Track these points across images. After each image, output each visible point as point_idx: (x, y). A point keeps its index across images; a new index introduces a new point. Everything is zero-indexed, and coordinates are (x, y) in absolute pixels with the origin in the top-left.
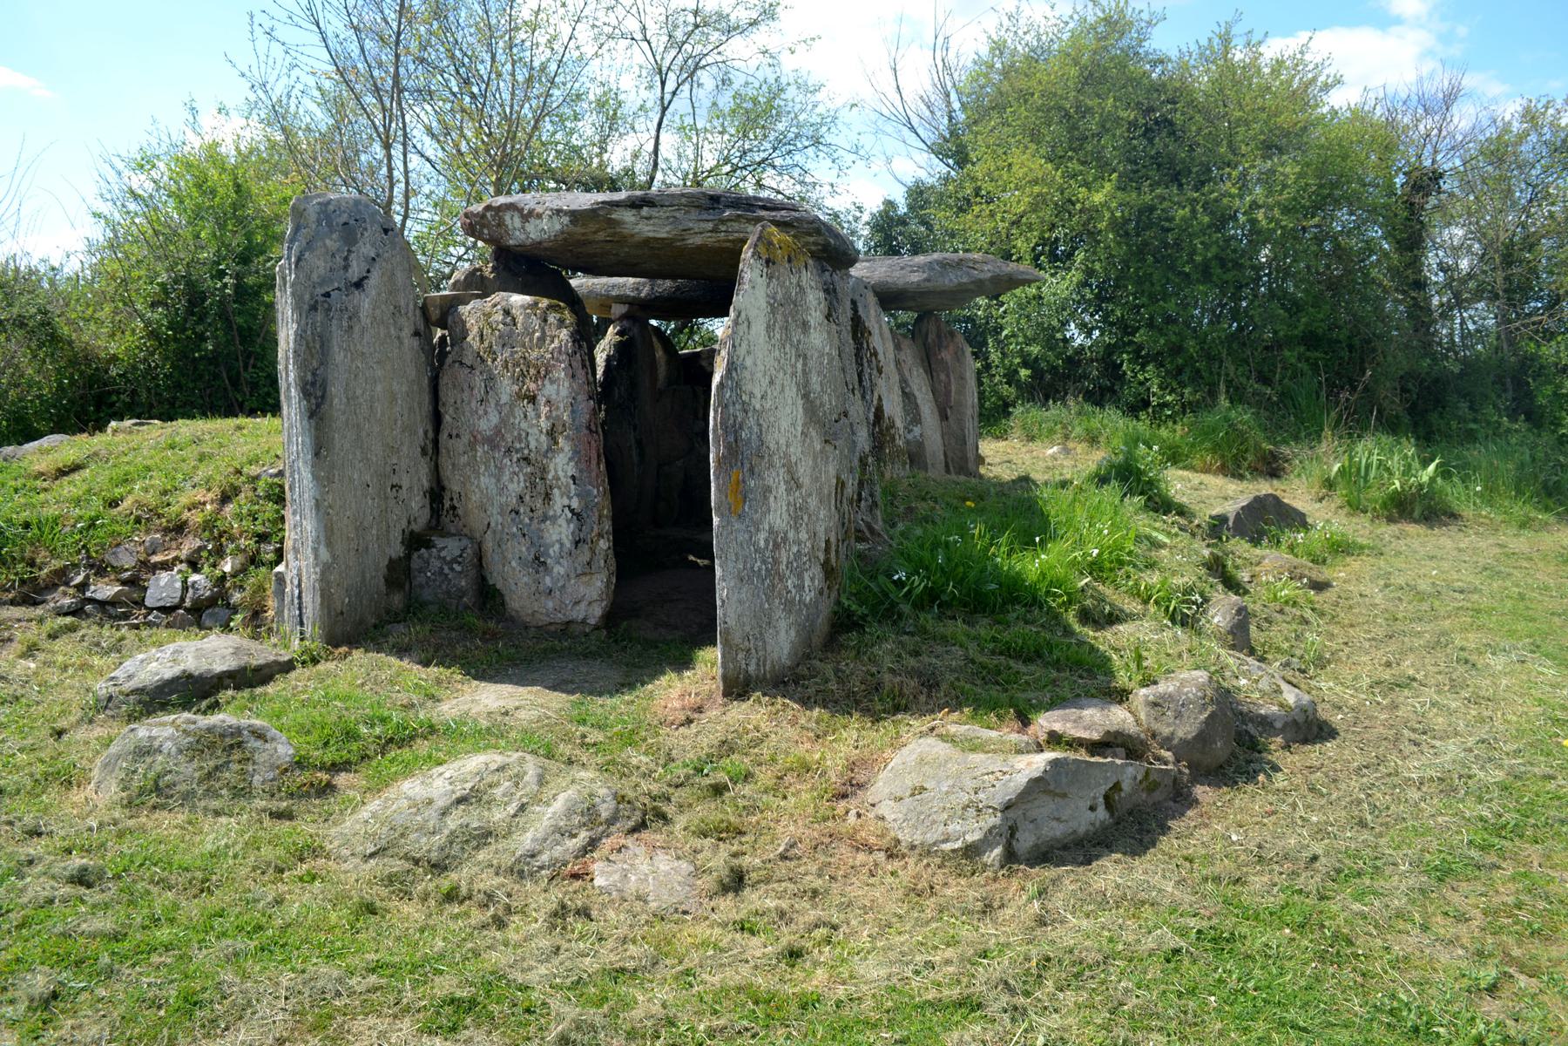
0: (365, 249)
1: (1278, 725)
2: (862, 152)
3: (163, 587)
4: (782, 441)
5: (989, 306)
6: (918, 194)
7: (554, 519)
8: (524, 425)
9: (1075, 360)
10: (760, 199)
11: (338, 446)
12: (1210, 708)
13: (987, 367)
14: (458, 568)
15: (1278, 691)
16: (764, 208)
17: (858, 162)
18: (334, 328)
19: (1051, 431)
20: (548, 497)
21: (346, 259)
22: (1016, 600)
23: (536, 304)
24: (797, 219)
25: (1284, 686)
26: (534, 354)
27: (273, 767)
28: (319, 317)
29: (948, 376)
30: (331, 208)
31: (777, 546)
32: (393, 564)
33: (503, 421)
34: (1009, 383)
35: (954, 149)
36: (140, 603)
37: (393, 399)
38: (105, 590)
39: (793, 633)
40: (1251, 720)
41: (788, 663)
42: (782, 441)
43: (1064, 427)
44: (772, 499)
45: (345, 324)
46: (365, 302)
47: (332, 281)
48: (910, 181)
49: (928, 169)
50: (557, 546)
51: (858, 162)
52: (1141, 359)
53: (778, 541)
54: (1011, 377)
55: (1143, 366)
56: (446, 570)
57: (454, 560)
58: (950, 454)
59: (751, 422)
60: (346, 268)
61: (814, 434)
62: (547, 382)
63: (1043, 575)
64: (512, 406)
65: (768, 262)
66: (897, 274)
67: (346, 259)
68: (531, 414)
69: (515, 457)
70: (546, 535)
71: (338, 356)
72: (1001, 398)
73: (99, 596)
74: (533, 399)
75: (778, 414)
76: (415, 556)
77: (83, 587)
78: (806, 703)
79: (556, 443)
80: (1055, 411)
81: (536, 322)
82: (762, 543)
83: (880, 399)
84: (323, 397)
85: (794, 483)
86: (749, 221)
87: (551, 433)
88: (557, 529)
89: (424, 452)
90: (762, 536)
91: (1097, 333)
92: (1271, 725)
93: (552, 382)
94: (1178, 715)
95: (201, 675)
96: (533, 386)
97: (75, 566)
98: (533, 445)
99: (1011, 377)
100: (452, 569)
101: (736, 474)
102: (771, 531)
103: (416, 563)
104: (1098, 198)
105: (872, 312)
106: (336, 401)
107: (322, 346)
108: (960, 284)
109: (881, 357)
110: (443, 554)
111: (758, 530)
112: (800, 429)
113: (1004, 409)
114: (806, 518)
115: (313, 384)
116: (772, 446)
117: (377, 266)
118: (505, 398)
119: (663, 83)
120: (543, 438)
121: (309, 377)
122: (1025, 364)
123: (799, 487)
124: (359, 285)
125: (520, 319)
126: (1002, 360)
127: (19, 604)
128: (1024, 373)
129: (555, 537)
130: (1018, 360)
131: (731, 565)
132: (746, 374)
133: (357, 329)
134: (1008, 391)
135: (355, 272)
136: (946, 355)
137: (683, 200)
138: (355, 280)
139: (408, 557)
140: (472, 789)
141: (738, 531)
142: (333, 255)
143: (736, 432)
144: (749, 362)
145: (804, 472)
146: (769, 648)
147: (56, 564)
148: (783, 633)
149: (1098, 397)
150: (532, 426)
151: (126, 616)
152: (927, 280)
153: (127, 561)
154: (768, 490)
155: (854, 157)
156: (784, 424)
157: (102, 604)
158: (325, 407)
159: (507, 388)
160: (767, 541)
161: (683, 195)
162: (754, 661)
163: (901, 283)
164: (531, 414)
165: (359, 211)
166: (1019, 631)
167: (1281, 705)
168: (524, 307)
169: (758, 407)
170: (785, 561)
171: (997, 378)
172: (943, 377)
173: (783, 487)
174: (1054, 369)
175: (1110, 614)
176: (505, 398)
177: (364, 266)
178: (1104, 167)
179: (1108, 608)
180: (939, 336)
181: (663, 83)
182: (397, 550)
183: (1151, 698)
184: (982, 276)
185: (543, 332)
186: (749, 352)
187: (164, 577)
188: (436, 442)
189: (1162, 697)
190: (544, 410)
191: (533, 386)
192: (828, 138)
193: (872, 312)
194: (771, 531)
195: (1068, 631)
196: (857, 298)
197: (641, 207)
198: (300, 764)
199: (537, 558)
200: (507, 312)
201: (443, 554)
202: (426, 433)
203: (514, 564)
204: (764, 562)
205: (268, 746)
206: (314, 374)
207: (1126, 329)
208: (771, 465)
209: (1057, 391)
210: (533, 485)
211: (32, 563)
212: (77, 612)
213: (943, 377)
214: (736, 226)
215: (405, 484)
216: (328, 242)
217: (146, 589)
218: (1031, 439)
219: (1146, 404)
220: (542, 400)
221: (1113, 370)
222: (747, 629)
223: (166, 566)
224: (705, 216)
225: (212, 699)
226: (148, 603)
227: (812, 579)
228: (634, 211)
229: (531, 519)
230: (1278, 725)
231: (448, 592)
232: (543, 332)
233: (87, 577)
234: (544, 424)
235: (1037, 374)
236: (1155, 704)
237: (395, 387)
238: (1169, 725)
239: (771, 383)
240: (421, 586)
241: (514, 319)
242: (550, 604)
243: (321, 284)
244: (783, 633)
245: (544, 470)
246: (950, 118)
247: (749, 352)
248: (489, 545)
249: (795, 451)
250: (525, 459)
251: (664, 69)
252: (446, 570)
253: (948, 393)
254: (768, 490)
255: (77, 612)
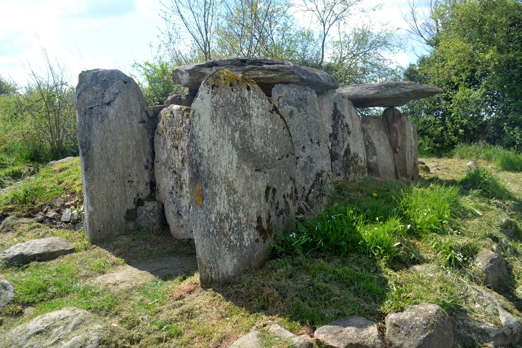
0: (113, 89)
1: (492, 335)
2: (402, 46)
3: (67, 214)
4: (223, 171)
5: (446, 104)
6: (423, 61)
7: (183, 196)
8: (174, 158)
9: (484, 125)
10: (267, 60)
11: (96, 166)
12: (429, 332)
13: (446, 129)
14: (152, 214)
15: (497, 314)
16: (268, 64)
17: (400, 50)
18: (93, 121)
19: (471, 155)
20: (181, 188)
21: (103, 94)
22: (355, 250)
23: (181, 109)
24: (281, 68)
25: (501, 312)
26: (178, 129)
27: (5, 301)
28: (87, 117)
29: (397, 134)
30: (99, 74)
31: (221, 220)
32: (129, 212)
33: (168, 156)
34: (455, 135)
35: (434, 43)
36: (60, 219)
37: (128, 147)
38: (51, 214)
39: (235, 261)
40: (475, 331)
41: (233, 274)
42: (223, 171)
43: (477, 154)
44: (217, 199)
45: (100, 119)
46: (111, 111)
47: (95, 103)
48: (420, 55)
49: (426, 51)
50: (185, 208)
51: (400, 50)
52: (513, 125)
53: (222, 218)
54: (456, 133)
55: (513, 128)
56: (148, 215)
57: (150, 211)
58: (398, 168)
59: (204, 162)
60: (103, 98)
61: (245, 167)
62: (181, 141)
63: (373, 239)
64: (171, 150)
65: (213, 87)
66: (364, 91)
67: (103, 94)
68: (176, 154)
69: (172, 171)
70: (181, 203)
71: (96, 132)
72: (452, 142)
73: (49, 216)
74: (177, 148)
75: (220, 158)
76: (138, 208)
77: (46, 212)
78: (228, 298)
79: (184, 166)
80: (473, 147)
81: (180, 116)
82: (213, 219)
83: (348, 145)
84: (89, 148)
85: (231, 190)
86: (259, 69)
87: (183, 161)
88: (185, 201)
89: (146, 167)
90: (213, 217)
91: (494, 114)
92: (487, 335)
93: (183, 141)
94: (408, 334)
95: (27, 255)
96: (177, 142)
97: (45, 205)
98: (177, 166)
99: (456, 133)
100: (150, 215)
101: (198, 187)
102: (218, 213)
103: (139, 212)
104: (488, 56)
105: (346, 108)
106: (95, 149)
107: (89, 128)
108: (394, 95)
109: (350, 127)
110: (146, 208)
111: (211, 213)
112: (235, 165)
113: (452, 145)
114: (241, 207)
115: (85, 143)
116: (217, 173)
117: (119, 96)
118: (169, 147)
119: (324, 26)
120: (180, 163)
121: (84, 140)
122: (462, 127)
123: (236, 192)
124: (109, 104)
125: (175, 115)
126: (452, 126)
127: (28, 217)
128: (461, 131)
129: (184, 204)
130: (458, 126)
131: (198, 228)
132: (200, 140)
133: (106, 121)
134: (454, 138)
135: (107, 99)
136: (396, 125)
137: (229, 62)
138: (107, 102)
139: (136, 209)
140: (46, 328)
141: (200, 213)
142: (97, 93)
143: (197, 167)
144: (200, 134)
145: (239, 185)
146: (220, 268)
147: (41, 203)
148: (228, 261)
149: (493, 141)
150: (176, 159)
151: (55, 224)
152: (377, 93)
153: (58, 204)
154: (215, 194)
155: (399, 48)
156: (224, 163)
157: (51, 219)
158: (90, 152)
159: (169, 143)
160: (216, 218)
161: (228, 60)
162: (214, 273)
163: (364, 95)
164: (176, 154)
165: (113, 75)
166: (352, 269)
167: (496, 324)
168: (177, 110)
169: (206, 155)
170: (228, 228)
171: (450, 133)
172: (395, 135)
173: (224, 193)
174: (474, 129)
175: (414, 259)
176: (169, 147)
177: (112, 97)
178: (491, 41)
179: (413, 255)
180: (393, 117)
181: (324, 26)
182: (131, 205)
183: (394, 321)
184: (406, 91)
185: (182, 121)
186: (200, 130)
187: (67, 210)
188: (153, 164)
189: (400, 321)
190: (180, 152)
191: (177, 142)
192: (390, 42)
193: (346, 108)
194: (218, 213)
195: (378, 270)
196: (337, 102)
197: (212, 67)
198: (14, 301)
199: (178, 212)
200: (172, 113)
201: (146, 208)
202: (148, 161)
203: (171, 214)
204: (215, 228)
205: (6, 292)
206: (86, 139)
207: (506, 113)
208: (217, 183)
209: (475, 138)
210: (177, 183)
211: (34, 203)
212: (41, 222)
213: (395, 135)
214: (253, 72)
215: (135, 180)
216: (94, 88)
217: (62, 214)
218: (463, 158)
219: (514, 143)
220: (179, 148)
221: (500, 129)
222: (208, 258)
223: (69, 207)
224: (239, 69)
225: (28, 265)
226: (62, 219)
227: (249, 235)
228: (209, 69)
229: (176, 196)
230: (492, 335)
231: (149, 223)
232: (182, 121)
233: (47, 209)
234: (180, 158)
235: (467, 131)
236: (395, 325)
237: (129, 143)
238: (400, 339)
239: (214, 144)
240: (140, 220)
241: (173, 115)
242: (183, 231)
243: (89, 104)
244: (228, 261)
245: (180, 177)
246: (438, 31)
247: (200, 130)
248: (165, 205)
249: (232, 176)
250: (175, 172)
251: (324, 21)
252: (148, 215)
253: (397, 142)
254: (215, 194)
255: (41, 222)
